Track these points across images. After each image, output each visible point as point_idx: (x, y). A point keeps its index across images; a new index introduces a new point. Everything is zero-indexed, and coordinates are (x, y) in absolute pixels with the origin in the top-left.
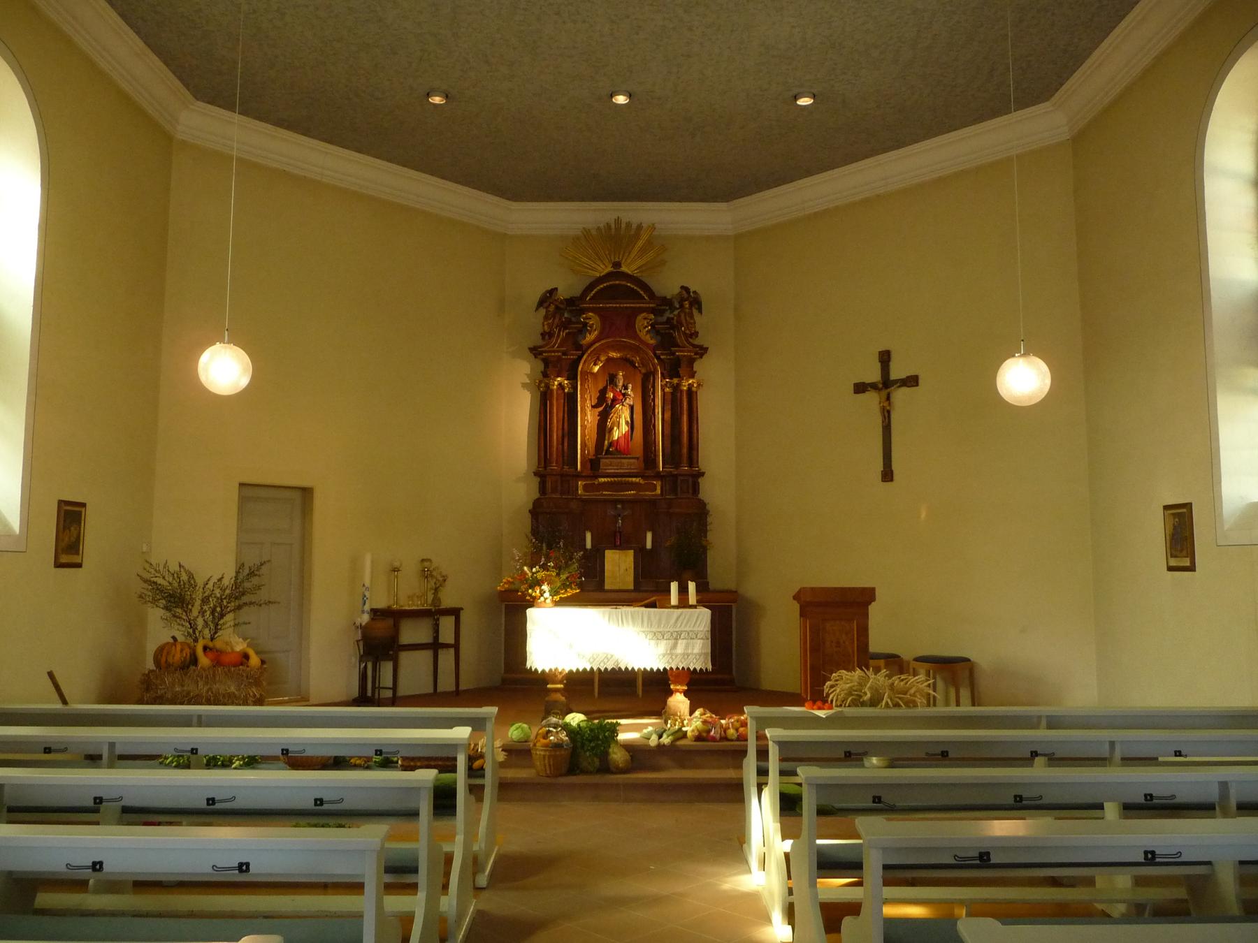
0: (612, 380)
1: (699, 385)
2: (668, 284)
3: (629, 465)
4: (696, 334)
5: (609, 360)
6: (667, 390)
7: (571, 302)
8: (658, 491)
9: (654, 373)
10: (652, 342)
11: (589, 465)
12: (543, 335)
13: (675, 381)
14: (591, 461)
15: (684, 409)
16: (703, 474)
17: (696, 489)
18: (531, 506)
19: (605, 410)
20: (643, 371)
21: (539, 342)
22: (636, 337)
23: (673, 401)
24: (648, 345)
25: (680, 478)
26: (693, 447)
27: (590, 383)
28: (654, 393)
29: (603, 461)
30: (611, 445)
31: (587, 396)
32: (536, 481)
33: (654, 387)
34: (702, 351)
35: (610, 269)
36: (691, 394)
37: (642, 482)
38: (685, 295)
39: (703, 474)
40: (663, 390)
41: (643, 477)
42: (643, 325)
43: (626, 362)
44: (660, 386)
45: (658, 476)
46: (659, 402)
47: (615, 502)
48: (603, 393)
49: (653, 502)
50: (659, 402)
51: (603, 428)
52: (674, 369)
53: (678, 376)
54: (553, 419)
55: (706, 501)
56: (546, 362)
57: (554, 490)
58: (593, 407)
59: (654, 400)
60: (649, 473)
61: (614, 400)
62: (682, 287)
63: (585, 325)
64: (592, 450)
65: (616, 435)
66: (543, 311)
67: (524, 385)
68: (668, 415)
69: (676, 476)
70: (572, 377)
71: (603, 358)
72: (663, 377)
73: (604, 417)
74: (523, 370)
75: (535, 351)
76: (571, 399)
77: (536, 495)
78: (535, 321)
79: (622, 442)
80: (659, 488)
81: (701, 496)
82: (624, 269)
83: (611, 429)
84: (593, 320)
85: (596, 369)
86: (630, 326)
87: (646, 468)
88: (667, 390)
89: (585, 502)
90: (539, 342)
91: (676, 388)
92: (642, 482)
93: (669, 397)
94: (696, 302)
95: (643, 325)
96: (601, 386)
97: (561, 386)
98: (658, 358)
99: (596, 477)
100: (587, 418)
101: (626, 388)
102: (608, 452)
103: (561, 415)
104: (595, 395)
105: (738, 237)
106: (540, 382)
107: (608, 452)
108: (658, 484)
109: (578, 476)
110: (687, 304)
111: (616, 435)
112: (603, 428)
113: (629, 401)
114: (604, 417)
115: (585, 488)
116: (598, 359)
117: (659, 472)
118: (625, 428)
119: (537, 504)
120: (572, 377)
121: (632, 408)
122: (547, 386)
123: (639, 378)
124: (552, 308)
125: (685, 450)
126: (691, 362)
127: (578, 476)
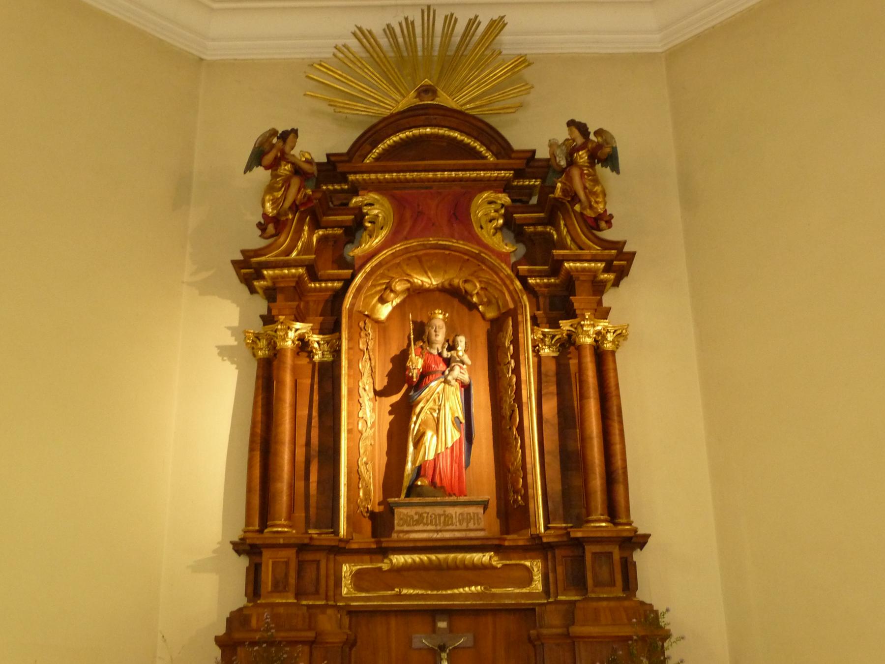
0: (421, 333)
1: (620, 336)
2: (537, 132)
3: (473, 520)
4: (608, 220)
5: (415, 293)
6: (546, 351)
7: (333, 168)
8: (537, 585)
9: (513, 314)
10: (508, 249)
11: (367, 525)
12: (262, 227)
13: (566, 325)
14: (373, 516)
15: (586, 389)
16: (639, 541)
17: (629, 581)
18: (221, 630)
19: (403, 387)
20: (491, 314)
21: (256, 241)
22: (474, 239)
23: (562, 377)
24: (504, 257)
25: (590, 549)
26: (614, 477)
27: (370, 339)
28: (516, 356)
29: (400, 512)
30: (419, 472)
31: (364, 366)
32: (242, 563)
33: (515, 342)
34: (620, 263)
35: (409, 100)
36: (602, 358)
37: (496, 562)
38: (580, 140)
39: (639, 541)
40: (536, 352)
41: (498, 549)
42: (487, 209)
43: (454, 295)
44: (534, 344)
45: (538, 547)
46: (528, 374)
47: (435, 613)
48: (401, 361)
49: (526, 613)
50: (528, 374)
51: (399, 434)
52: (559, 305)
53: (571, 314)
54: (289, 425)
55: (659, 606)
56: (271, 294)
57: (279, 586)
58: (378, 394)
59: (517, 371)
60: (511, 540)
61: (426, 374)
62: (571, 123)
63: (360, 217)
64: (376, 495)
65: (431, 446)
66: (261, 174)
67: (225, 352)
68: (550, 406)
69: (579, 543)
70: (331, 327)
71: (399, 287)
72: (535, 322)
73: (403, 414)
74: (227, 315)
75: (248, 269)
76: (328, 377)
77: (238, 599)
78: (245, 199)
79: (445, 464)
80: (538, 578)
81: (644, 594)
82: (445, 99)
83: (419, 440)
84: (377, 208)
85: (384, 311)
86: (459, 216)
87: (506, 529)
88: (546, 351)
89: (353, 613)
90: (256, 241)
91: (568, 345)
92: (496, 562)
93: (550, 368)
94: (604, 154)
95: (487, 209)
96: (395, 351)
97: (303, 345)
98: (523, 280)
99: (384, 552)
100: (364, 417)
101: (452, 347)
102: (412, 490)
103: (303, 412)
104: (384, 368)
105: (673, 55)
106: (257, 337)
107: (412, 490)
108: (536, 566)
109: (341, 550)
110: (582, 157)
111: (431, 446)
112: (399, 434)
113: (459, 373)
114: (403, 414)
115: (359, 578)
116: (389, 288)
117: (539, 537)
118: (453, 435)
119: (237, 620)
120: (331, 327)
121: (466, 389)
122: (272, 345)
123: (481, 330)
124: (285, 169)
125: (597, 482)
126: (599, 288)
127: (341, 550)
